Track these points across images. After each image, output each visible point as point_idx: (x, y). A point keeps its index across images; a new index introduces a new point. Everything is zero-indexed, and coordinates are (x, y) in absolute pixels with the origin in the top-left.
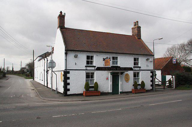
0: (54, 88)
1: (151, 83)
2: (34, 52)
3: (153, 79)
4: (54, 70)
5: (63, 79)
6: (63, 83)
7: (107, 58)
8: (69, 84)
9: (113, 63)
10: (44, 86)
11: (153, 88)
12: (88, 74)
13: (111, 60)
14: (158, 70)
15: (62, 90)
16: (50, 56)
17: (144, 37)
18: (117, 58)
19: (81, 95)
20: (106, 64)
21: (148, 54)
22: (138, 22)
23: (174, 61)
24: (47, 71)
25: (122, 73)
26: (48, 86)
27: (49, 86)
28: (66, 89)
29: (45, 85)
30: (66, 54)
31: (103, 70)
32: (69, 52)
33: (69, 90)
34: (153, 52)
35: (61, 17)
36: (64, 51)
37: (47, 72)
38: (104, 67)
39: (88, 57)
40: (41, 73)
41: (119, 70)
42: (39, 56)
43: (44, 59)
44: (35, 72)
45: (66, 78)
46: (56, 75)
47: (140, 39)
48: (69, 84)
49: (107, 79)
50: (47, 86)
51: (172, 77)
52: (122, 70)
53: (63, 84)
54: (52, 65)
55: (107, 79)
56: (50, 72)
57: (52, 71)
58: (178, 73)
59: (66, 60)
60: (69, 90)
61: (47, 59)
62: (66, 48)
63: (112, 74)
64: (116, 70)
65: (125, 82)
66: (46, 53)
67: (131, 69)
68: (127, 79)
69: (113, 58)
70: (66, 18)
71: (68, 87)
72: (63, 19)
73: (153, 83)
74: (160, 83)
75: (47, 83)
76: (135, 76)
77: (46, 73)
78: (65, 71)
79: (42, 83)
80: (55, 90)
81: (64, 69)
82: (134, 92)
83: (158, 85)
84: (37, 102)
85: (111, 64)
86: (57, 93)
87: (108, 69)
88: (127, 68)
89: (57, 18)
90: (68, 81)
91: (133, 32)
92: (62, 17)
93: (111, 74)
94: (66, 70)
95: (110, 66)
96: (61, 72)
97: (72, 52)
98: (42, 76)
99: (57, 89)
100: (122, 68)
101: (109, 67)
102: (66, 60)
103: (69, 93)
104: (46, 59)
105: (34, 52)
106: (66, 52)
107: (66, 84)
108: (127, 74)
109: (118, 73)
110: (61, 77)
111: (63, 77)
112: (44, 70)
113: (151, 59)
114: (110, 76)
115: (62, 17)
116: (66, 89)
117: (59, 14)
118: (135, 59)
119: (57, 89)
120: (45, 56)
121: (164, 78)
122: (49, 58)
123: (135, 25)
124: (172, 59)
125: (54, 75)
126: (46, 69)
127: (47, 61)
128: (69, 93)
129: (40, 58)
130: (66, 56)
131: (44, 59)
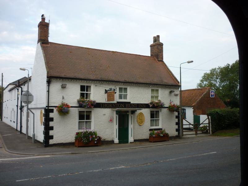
0: (31, 134)
1: (177, 127)
2: (2, 76)
3: (179, 120)
4: (30, 106)
5: (43, 121)
6: (43, 127)
7: (111, 89)
8: (52, 128)
9: (120, 97)
11: (179, 133)
12: (82, 114)
13: (116, 93)
14: (189, 106)
15: (41, 137)
16: (26, 85)
17: (168, 58)
18: (126, 89)
20: (109, 98)
21: (174, 85)
22: (158, 36)
23: (212, 93)
24: (22, 108)
25: (133, 112)
27: (24, 131)
28: (48, 137)
30: (49, 82)
33: (52, 137)
34: (180, 81)
36: (45, 79)
37: (21, 111)
38: (107, 103)
40: (13, 109)
41: (129, 108)
42: (10, 84)
43: (18, 89)
44: (4, 108)
45: (48, 120)
46: (34, 114)
47: (162, 61)
48: (52, 128)
50: (21, 131)
51: (208, 118)
53: (42, 128)
54: (27, 98)
55: (111, 121)
56: (25, 109)
57: (28, 109)
58: (218, 111)
59: (48, 91)
60: (52, 137)
61: (22, 88)
63: (118, 112)
65: (137, 125)
66: (20, 79)
67: (146, 106)
68: (141, 122)
69: (121, 89)
70: (51, 28)
71: (51, 133)
72: (46, 28)
73: (179, 127)
74: (191, 126)
75: (21, 127)
76: (152, 115)
77: (19, 111)
78: (47, 108)
79: (14, 125)
81: (44, 105)
83: (189, 129)
84: (67, 154)
85: (117, 99)
87: (112, 106)
88: (141, 104)
89: (37, 26)
92: (44, 27)
93: (117, 114)
94: (48, 106)
95: (115, 102)
96: (41, 110)
97: (58, 79)
98: (14, 114)
99: (34, 135)
100: (133, 104)
101: (114, 104)
102: (48, 91)
103: (51, 142)
104: (20, 89)
105: (2, 76)
106: (49, 80)
107: (48, 129)
108: (141, 114)
109: (128, 112)
110: (41, 117)
111: (44, 118)
112: (17, 106)
113: (177, 92)
114: (115, 117)
115: (44, 27)
116: (48, 137)
117: (40, 20)
120: (19, 84)
121: (197, 119)
122: (25, 88)
124: (209, 91)
125: (31, 115)
126: (19, 105)
127: (22, 91)
130: (49, 86)
131: (18, 89)
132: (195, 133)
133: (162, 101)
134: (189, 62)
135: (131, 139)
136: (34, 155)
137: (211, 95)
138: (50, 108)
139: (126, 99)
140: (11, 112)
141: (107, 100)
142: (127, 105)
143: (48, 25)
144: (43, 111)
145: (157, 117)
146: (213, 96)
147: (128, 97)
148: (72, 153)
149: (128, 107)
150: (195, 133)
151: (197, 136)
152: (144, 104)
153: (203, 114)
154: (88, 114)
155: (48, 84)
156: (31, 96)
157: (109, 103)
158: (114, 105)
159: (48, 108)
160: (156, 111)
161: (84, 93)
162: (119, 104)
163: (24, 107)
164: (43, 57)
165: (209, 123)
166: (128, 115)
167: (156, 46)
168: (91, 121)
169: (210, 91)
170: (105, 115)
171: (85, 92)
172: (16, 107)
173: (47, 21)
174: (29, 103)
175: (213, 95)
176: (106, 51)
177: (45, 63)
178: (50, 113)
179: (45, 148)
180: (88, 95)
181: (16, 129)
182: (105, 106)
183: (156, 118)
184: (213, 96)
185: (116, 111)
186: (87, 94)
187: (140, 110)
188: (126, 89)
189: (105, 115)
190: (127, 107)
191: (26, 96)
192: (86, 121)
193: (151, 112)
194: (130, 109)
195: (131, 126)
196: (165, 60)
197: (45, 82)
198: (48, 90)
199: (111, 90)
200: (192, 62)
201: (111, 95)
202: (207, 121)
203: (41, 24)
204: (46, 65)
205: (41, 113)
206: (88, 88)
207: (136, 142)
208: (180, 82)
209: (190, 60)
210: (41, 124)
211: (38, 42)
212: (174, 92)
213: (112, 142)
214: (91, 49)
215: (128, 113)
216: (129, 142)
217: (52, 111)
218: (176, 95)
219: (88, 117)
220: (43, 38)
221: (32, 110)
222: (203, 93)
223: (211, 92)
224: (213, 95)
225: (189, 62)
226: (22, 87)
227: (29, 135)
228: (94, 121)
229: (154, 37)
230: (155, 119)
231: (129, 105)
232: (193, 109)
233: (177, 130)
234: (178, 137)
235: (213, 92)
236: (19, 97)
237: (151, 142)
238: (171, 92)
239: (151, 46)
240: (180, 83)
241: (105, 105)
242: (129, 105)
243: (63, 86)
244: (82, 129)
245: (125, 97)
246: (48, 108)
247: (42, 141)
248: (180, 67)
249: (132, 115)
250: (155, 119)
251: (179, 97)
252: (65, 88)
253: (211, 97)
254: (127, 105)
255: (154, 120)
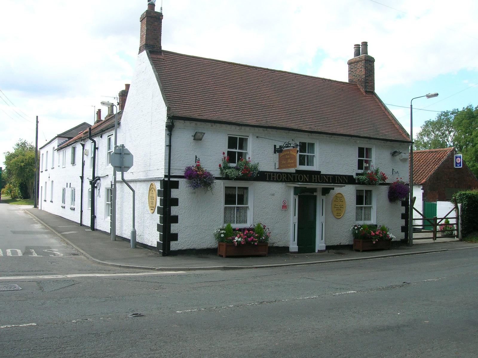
0: (127, 235)
1: (403, 222)
2: (37, 122)
4: (128, 176)
5: (158, 204)
8: (175, 219)
10: (81, 224)
11: (406, 235)
12: (230, 192)
19: (349, 247)
20: (284, 162)
25: (326, 191)
26: (98, 226)
29: (84, 223)
30: (170, 128)
31: (273, 181)
32: (178, 124)
33: (175, 237)
35: (151, 17)
38: (277, 173)
39: (232, 142)
41: (318, 182)
42: (59, 136)
43: (83, 145)
48: (175, 219)
49: (285, 207)
51: (456, 207)
52: (326, 183)
53: (157, 218)
55: (285, 207)
59: (169, 146)
60: (175, 237)
61: (94, 142)
62: (169, 110)
63: (297, 191)
64: (310, 181)
67: (349, 180)
69: (303, 147)
70: (165, 23)
71: (174, 228)
72: (156, 23)
76: (360, 200)
77: (87, 187)
78: (166, 179)
80: (128, 240)
81: (161, 174)
82: (223, 251)
86: (136, 247)
88: (340, 176)
89: (139, 20)
90: (174, 211)
91: (351, 71)
93: (295, 194)
94: (168, 176)
95: (293, 170)
96: (150, 183)
99: (134, 233)
100: (326, 175)
103: (174, 246)
105: (37, 122)
109: (315, 190)
110: (151, 198)
111: (158, 199)
112: (82, 178)
114: (293, 200)
117: (146, 8)
118: (361, 152)
119: (134, 233)
123: (357, 53)
128: (174, 246)
129: (63, 140)
131: (74, 149)
132: (432, 236)
133: (382, 170)
134: (429, 96)
135: (320, 244)
136: (152, 269)
137: (456, 163)
138: (172, 179)
139: (313, 166)
140: (64, 190)
141: (277, 166)
142: (315, 177)
143: (161, 17)
144: (158, 186)
145: (369, 203)
146: (460, 166)
147: (316, 161)
148: (225, 269)
149: (316, 181)
150: (432, 236)
151: (436, 241)
152: (345, 176)
153: (444, 198)
154: (241, 193)
155: (168, 132)
156: (128, 155)
157: (282, 173)
158: (291, 176)
159: (169, 179)
160: (366, 191)
161: (235, 152)
162: (300, 176)
163: (99, 179)
164: (155, 79)
165: (457, 218)
166: (315, 198)
167: (360, 63)
168: (247, 207)
169: (453, 156)
170: (273, 195)
171: (238, 150)
172: (81, 180)
173: (157, 9)
174: (126, 169)
175: (460, 163)
176: (268, 69)
177: (162, 90)
178: (172, 190)
179: (163, 258)
180: (244, 155)
181: (80, 222)
182: (273, 178)
183: (365, 205)
184: (460, 166)
185: (295, 188)
186: (240, 154)
187: (345, 186)
188: (312, 145)
189: (273, 195)
190: (315, 180)
191: (119, 155)
192: (237, 207)
193: (358, 191)
194: (320, 186)
195: (320, 220)
196: (378, 90)
197: (164, 127)
198: (168, 144)
199: (288, 147)
200: (436, 95)
201: (287, 157)
202: (453, 214)
203: (149, 15)
204: (161, 91)
205: (151, 189)
206: (242, 143)
207: (330, 251)
208: (410, 134)
209: (433, 93)
210: (150, 212)
211: (141, 51)
212: (400, 153)
213: (283, 251)
214: (239, 65)
215: (315, 194)
216: (317, 251)
217: (176, 185)
218: (404, 160)
219: (242, 200)
220: (152, 43)
221: (132, 185)
222: (440, 159)
223: (456, 157)
224: (460, 163)
225: (429, 96)
226: (95, 139)
227: (116, 234)
228: (254, 207)
229: (355, 45)
230: (364, 205)
231: (317, 177)
232: (422, 189)
233: (405, 229)
234: (406, 243)
235: (460, 157)
236: (85, 159)
237: (358, 251)
238: (394, 154)
239: (350, 63)
240: (410, 137)
241: (273, 175)
242: (317, 177)
243: (196, 137)
244: (368, 204)
245: (310, 162)
246: (169, 179)
247: (155, 245)
248: (411, 106)
249: (324, 197)
250: (364, 205)
251: (407, 165)
252: (201, 140)
253: (461, 167)
254: (315, 177)
255: (362, 207)
